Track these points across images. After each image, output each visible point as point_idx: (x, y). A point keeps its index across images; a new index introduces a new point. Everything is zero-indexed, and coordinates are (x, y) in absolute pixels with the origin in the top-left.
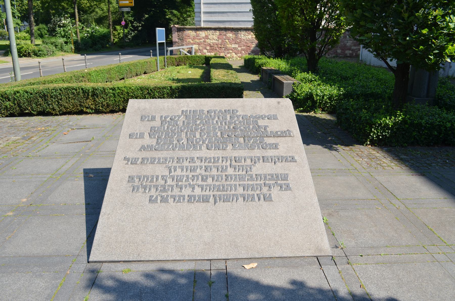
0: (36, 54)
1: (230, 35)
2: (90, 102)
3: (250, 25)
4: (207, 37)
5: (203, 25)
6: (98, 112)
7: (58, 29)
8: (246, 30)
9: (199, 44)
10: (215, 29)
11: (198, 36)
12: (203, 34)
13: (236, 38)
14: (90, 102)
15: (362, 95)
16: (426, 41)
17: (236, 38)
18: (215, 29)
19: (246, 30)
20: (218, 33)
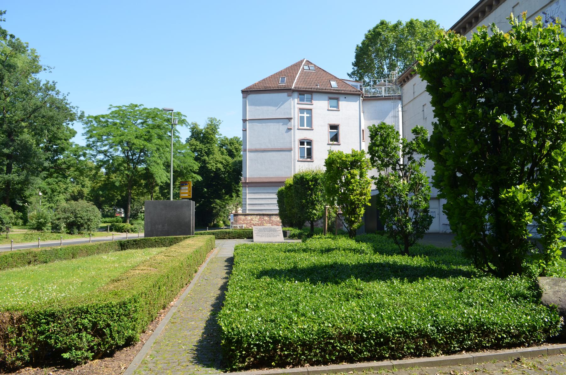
0: (133, 231)
1: (266, 218)
2: (227, 235)
3: (277, 212)
4: (252, 220)
5: (247, 212)
6: (229, 238)
7: (139, 214)
8: (276, 215)
9: (247, 224)
10: (257, 215)
11: (246, 219)
12: (249, 218)
13: (270, 220)
14: (227, 235)
15: (479, 328)
16: (310, 216)
17: (270, 220)
18: (257, 215)
19: (276, 215)
20: (258, 217)
